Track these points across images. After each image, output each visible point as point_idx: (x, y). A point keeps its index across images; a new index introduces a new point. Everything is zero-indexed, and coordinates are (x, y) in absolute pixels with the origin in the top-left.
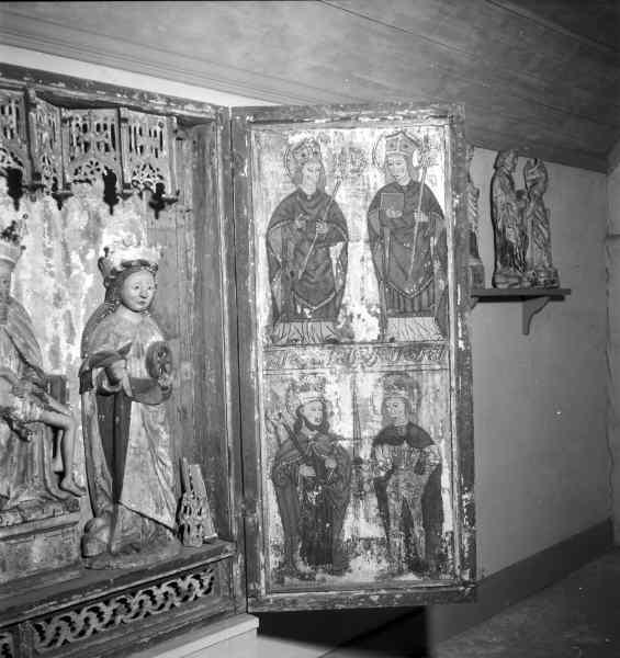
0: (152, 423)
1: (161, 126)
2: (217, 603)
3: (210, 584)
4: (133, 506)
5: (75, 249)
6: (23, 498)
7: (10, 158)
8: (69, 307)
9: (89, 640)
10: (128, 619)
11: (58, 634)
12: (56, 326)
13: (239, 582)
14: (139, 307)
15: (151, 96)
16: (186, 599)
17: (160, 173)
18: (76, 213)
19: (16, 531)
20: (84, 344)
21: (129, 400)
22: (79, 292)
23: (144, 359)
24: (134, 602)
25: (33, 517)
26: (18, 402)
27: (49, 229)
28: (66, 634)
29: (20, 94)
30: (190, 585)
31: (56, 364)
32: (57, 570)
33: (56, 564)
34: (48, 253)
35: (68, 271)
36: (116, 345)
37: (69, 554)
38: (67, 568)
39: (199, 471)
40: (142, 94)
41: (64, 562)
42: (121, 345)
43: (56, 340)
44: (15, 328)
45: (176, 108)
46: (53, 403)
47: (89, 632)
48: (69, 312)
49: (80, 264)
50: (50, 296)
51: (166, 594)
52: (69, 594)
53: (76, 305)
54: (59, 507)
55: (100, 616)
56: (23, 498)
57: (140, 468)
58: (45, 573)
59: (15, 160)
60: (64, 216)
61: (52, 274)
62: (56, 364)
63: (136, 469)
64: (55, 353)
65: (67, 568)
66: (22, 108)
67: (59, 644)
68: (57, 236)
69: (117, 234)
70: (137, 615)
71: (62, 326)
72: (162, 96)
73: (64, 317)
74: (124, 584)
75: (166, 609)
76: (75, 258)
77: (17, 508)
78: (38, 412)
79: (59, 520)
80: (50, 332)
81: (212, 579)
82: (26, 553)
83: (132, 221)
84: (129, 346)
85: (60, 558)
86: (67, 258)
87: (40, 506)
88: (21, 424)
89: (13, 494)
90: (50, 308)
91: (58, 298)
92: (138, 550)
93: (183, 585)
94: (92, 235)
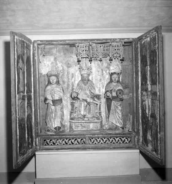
0: (116, 105)
1: (120, 44)
2: (131, 145)
3: (130, 141)
4: (111, 121)
5: (104, 70)
6: (88, 116)
7: (86, 55)
8: (103, 81)
9: (100, 144)
10: (109, 142)
11: (94, 141)
12: (100, 85)
13: (136, 142)
14: (115, 82)
15: (116, 39)
16: (123, 142)
17: (120, 54)
18: (105, 64)
19: (87, 121)
20: (105, 89)
21: (111, 100)
22: (105, 79)
23: (115, 92)
24: (117, 139)
25: (90, 119)
26: (88, 99)
27: (99, 67)
28: (95, 142)
29: (89, 43)
30: (125, 140)
31: (100, 92)
32: (95, 130)
33: (95, 129)
34: (98, 71)
35: (103, 75)
36: (110, 89)
37: (98, 128)
38: (97, 130)
39: (132, 117)
40: (114, 39)
41: (97, 129)
42: (111, 89)
43: (100, 88)
44: (89, 86)
45: (122, 40)
46: (96, 99)
47: (100, 143)
48: (103, 83)
49: (105, 73)
50: (99, 79)
51: (118, 140)
52: (95, 134)
53: (104, 81)
54: (95, 119)
55: (103, 140)
56: (88, 116)
57: (113, 114)
58: (92, 130)
59: (88, 56)
60: (102, 64)
61: (99, 76)
62: (100, 92)
63: (112, 114)
64: (99, 90)
65: (97, 130)
66: (89, 46)
67: (94, 143)
68: (100, 68)
69: (114, 67)
70: (111, 142)
71: (101, 85)
72: (118, 39)
73: (101, 83)
74: (25, 134)
75: (118, 143)
76: (104, 72)
77: (87, 118)
78: (92, 101)
79: (95, 121)
80: (99, 86)
81: (131, 140)
82: (89, 126)
83: (118, 64)
84: (112, 89)
85: (96, 128)
86: (102, 72)
87: (92, 118)
88: (89, 103)
89: (87, 115)
90: (99, 82)
91: (101, 80)
92: (112, 130)
93: (123, 139)
94: (108, 68)
